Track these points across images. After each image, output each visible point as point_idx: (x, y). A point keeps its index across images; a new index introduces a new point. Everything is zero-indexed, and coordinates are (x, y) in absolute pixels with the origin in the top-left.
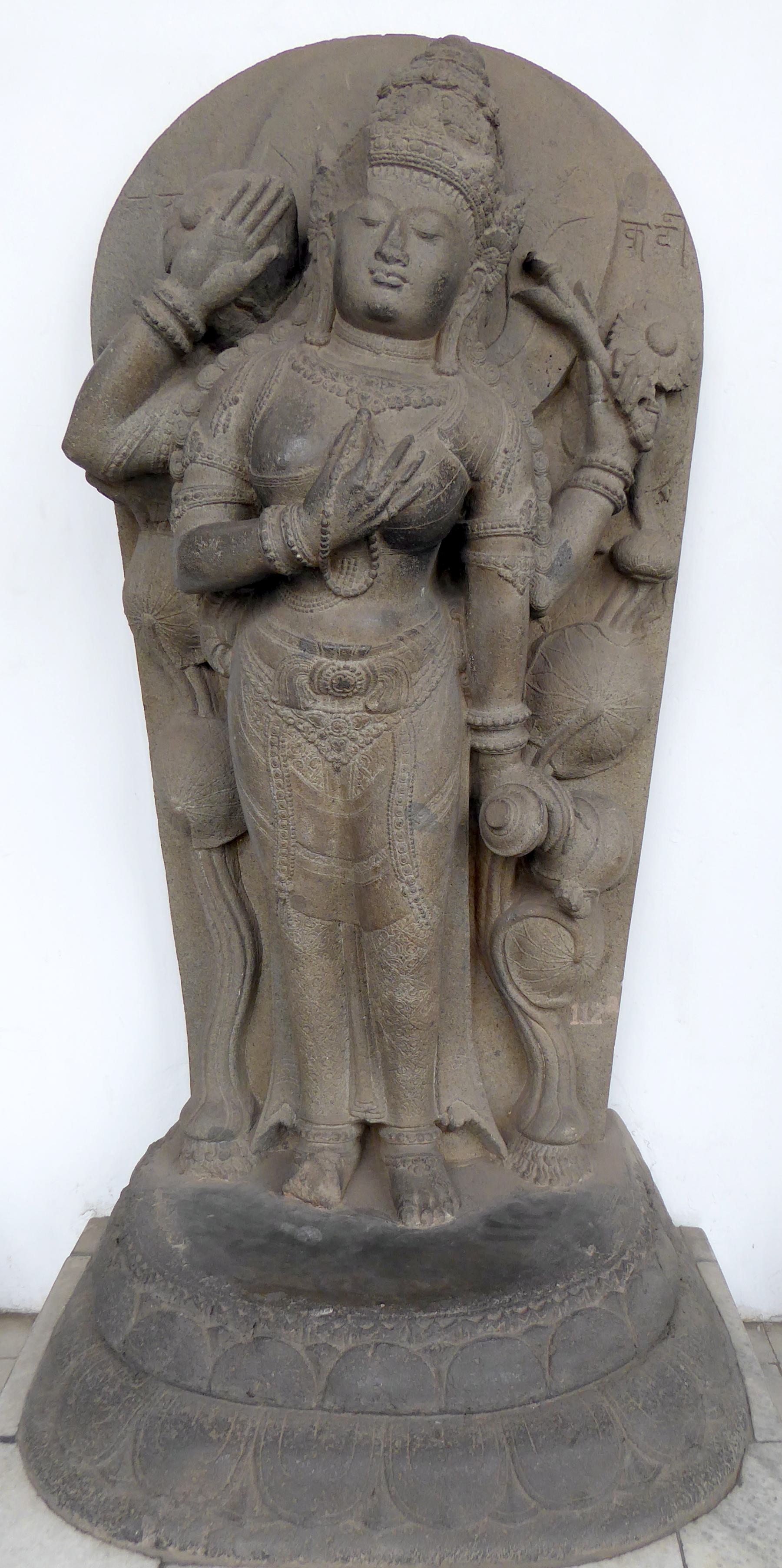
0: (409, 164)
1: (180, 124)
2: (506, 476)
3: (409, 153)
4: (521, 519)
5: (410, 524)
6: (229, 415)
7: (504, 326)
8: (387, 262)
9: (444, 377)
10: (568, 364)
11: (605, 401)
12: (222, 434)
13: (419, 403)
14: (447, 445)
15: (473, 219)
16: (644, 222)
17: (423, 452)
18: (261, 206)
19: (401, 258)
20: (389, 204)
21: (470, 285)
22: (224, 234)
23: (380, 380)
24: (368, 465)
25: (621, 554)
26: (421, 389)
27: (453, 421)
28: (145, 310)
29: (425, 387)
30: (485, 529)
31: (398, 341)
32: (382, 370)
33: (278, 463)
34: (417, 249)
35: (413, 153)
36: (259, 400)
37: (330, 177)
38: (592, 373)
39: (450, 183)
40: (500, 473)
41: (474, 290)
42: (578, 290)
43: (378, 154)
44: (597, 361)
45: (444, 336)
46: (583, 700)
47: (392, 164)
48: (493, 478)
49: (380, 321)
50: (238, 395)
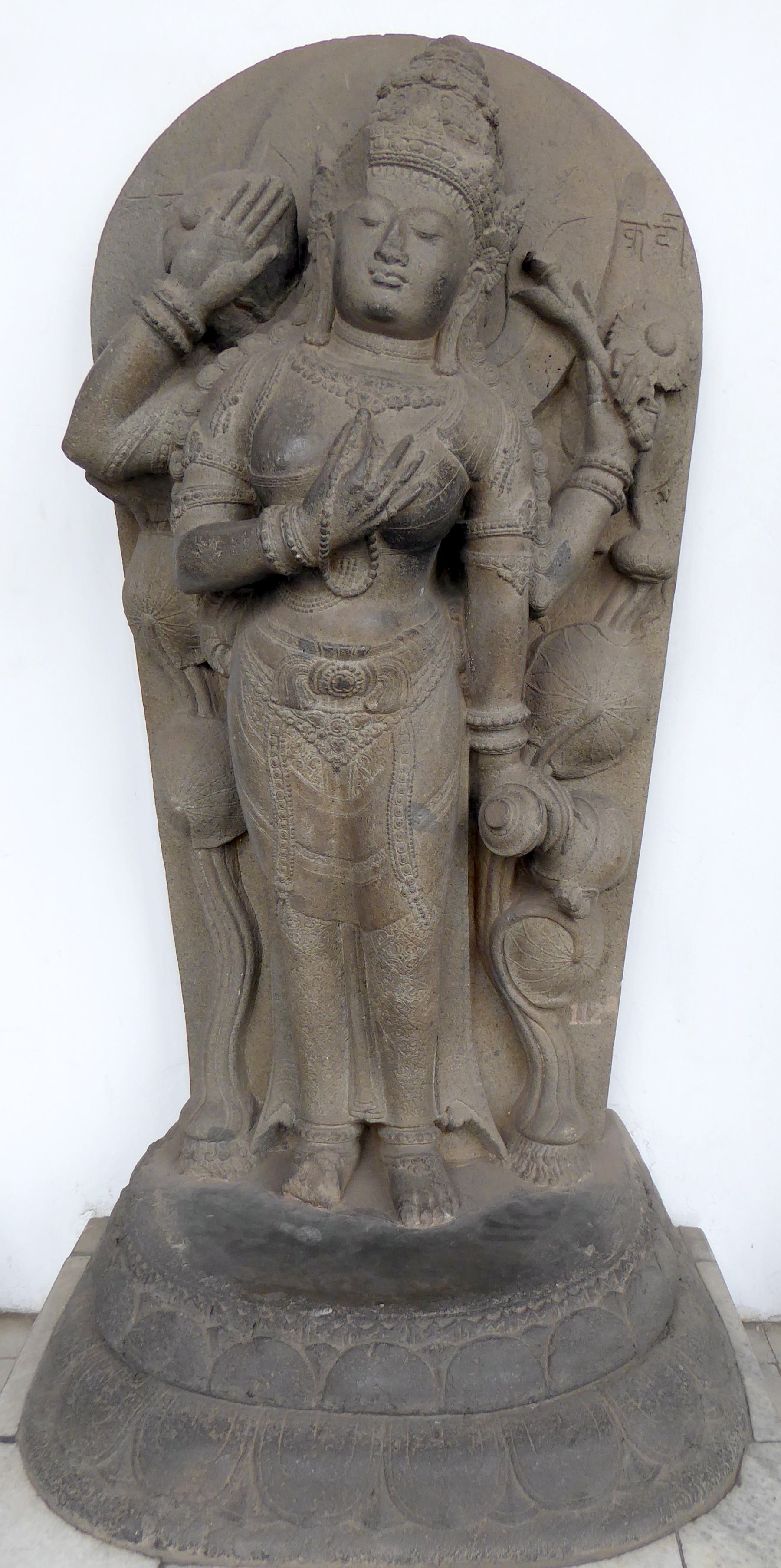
0: (408, 164)
1: (180, 124)
2: (506, 476)
3: (408, 153)
4: (520, 519)
5: (409, 524)
6: (229, 415)
7: (504, 326)
8: (386, 262)
9: (443, 377)
10: (567, 364)
11: (605, 401)
12: (222, 434)
13: (419, 403)
14: (447, 445)
15: (472, 219)
16: (643, 222)
17: (422, 452)
18: (261, 206)
19: (401, 258)
20: (389, 204)
21: (470, 285)
22: (224, 234)
23: (379, 380)
24: (368, 465)
25: (621, 554)
26: (421, 389)
27: (453, 421)
28: (145, 310)
29: (424, 387)
30: (484, 529)
31: (398, 341)
32: (382, 370)
33: (278, 463)
34: (417, 249)
35: (413, 153)
36: (258, 400)
37: (329, 177)
38: (591, 373)
39: (449, 183)
40: (499, 473)
41: (473, 290)
42: (578, 290)
43: (378, 154)
44: (596, 361)
45: (443, 336)
46: (582, 700)
47: (392, 164)
48: (492, 478)
49: (380, 321)
50: (238, 395)
